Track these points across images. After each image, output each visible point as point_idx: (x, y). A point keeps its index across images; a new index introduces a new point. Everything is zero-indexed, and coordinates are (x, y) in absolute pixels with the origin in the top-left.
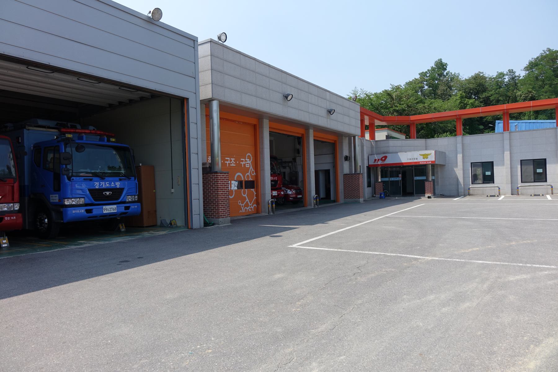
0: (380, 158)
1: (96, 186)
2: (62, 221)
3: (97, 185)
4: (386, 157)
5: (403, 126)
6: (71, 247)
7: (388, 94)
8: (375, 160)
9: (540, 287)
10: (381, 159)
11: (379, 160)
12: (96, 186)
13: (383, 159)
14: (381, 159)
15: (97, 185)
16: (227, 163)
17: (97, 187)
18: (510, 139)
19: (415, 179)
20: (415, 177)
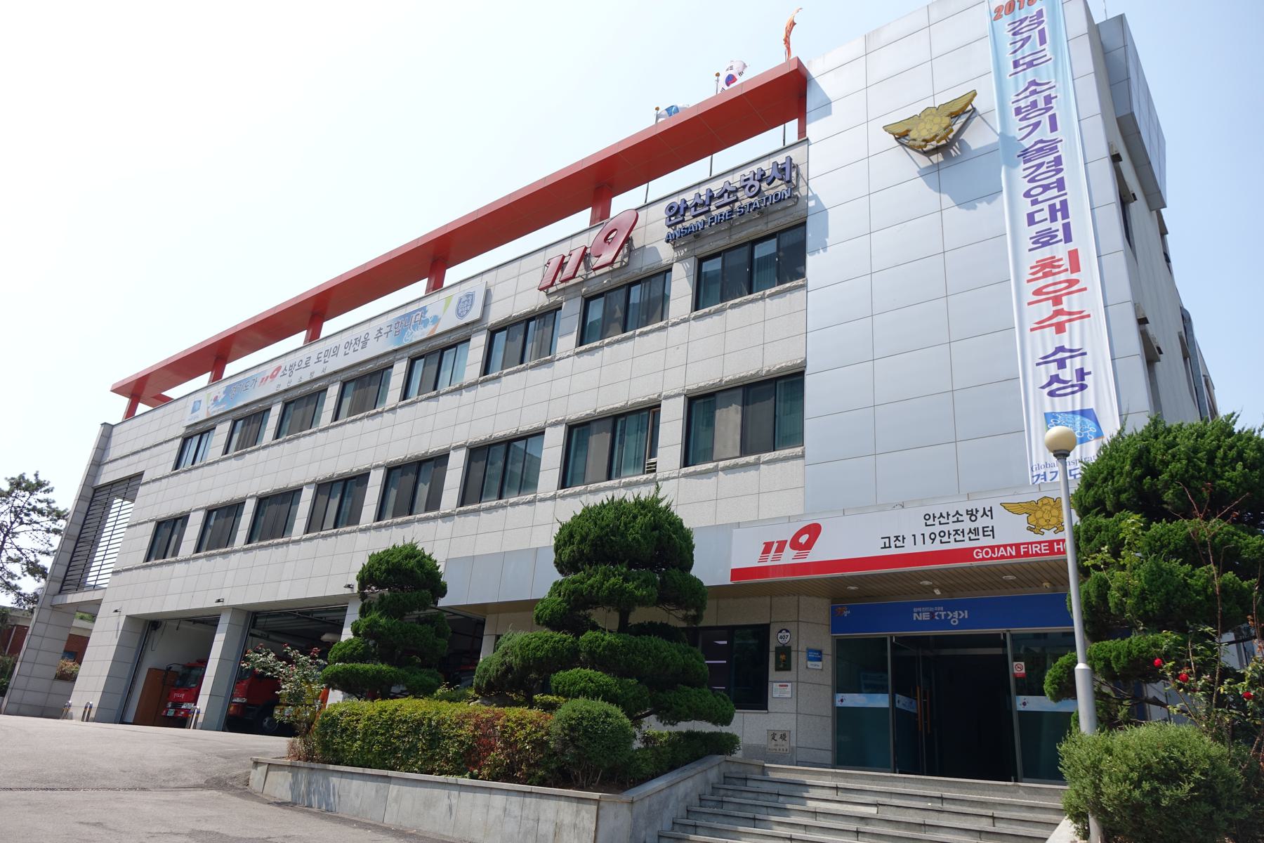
0: (789, 537)
1: (951, 619)
2: (694, 626)
3: (953, 617)
4: (814, 531)
5: (710, 226)
6: (345, 512)
7: (387, 551)
8: (768, 547)
9: (639, 759)
10: (795, 544)
11: (782, 545)
12: (951, 619)
13: (804, 539)
14: (795, 544)
15: (953, 617)
16: (1024, 552)
17: (955, 622)
18: (650, 287)
19: (1020, 708)
20: (1021, 699)
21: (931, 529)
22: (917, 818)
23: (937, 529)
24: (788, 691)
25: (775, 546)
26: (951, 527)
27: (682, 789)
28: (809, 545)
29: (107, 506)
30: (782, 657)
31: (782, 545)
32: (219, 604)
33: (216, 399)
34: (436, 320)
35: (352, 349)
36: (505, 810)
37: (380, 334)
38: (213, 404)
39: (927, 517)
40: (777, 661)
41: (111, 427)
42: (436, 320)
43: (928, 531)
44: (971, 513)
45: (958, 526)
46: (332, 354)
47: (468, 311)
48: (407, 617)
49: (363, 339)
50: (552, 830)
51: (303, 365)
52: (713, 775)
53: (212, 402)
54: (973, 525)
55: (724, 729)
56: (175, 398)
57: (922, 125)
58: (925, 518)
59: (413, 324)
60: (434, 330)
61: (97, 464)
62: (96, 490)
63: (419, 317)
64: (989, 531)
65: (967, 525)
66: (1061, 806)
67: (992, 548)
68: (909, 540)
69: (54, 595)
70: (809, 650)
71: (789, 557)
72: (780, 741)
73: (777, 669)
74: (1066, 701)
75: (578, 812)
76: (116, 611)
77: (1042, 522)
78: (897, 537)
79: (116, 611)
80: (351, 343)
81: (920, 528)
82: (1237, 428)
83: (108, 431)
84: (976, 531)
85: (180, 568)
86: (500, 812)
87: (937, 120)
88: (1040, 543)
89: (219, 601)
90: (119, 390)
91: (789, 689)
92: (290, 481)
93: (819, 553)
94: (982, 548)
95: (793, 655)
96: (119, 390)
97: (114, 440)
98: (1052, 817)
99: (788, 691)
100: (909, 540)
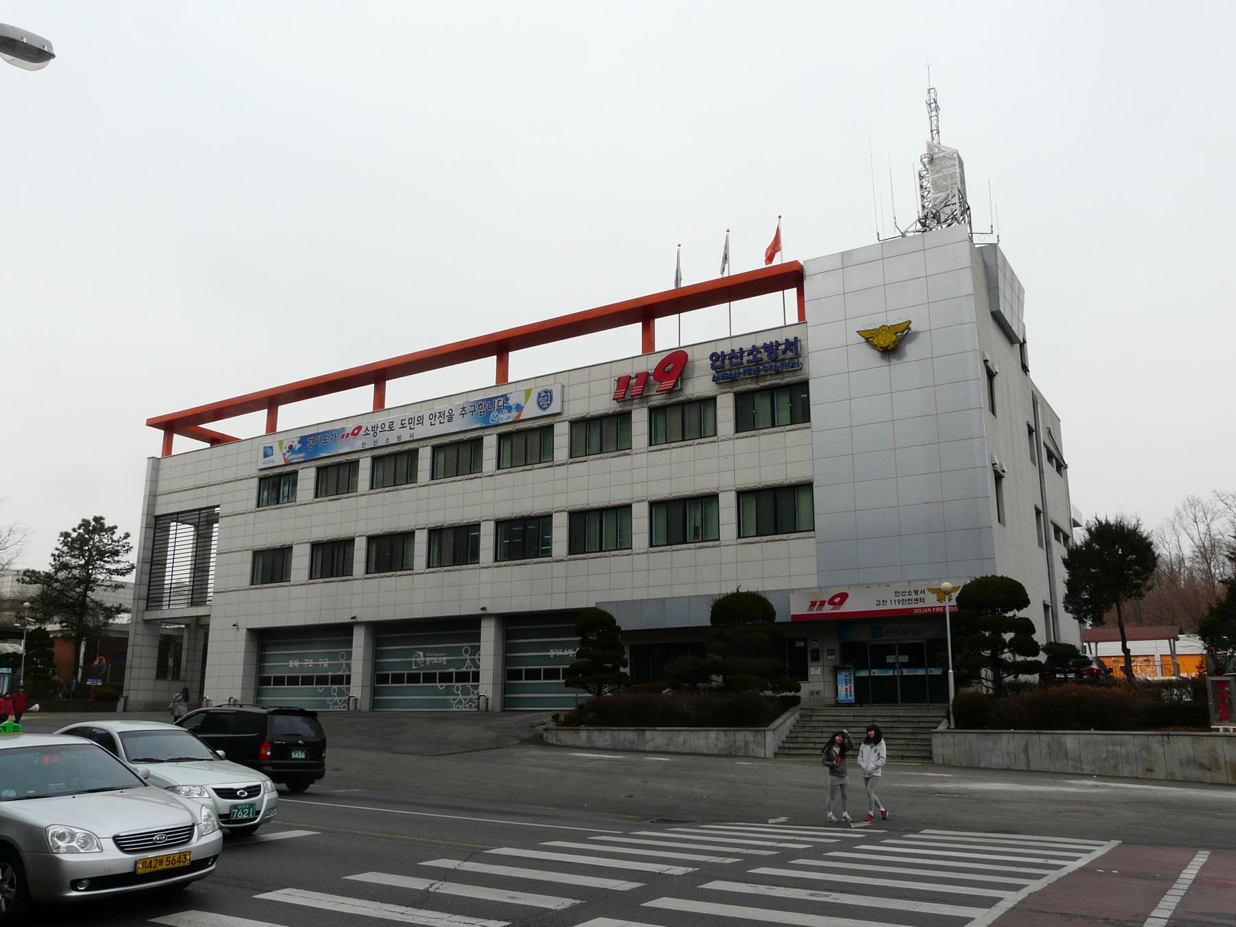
4: (844, 596)
8: (813, 604)
10: (831, 602)
11: (822, 603)
14: (831, 602)
21: (897, 598)
22: (890, 725)
23: (901, 598)
24: (819, 671)
25: (818, 603)
26: (907, 597)
27: (788, 723)
28: (841, 603)
29: (167, 530)
30: (815, 654)
31: (822, 603)
32: (354, 620)
33: (291, 447)
34: (519, 408)
35: (437, 421)
36: (717, 738)
37: (464, 412)
38: (288, 452)
39: (896, 592)
40: (812, 657)
41: (157, 461)
42: (519, 408)
43: (897, 598)
44: (916, 592)
45: (910, 597)
46: (416, 422)
47: (548, 405)
48: (188, 580)
49: (447, 414)
50: (743, 744)
51: (387, 428)
52: (797, 716)
53: (288, 449)
54: (916, 597)
55: (797, 694)
56: (243, 439)
57: (880, 337)
58: (384, 424)
59: (496, 407)
60: (519, 416)
61: (152, 496)
62: (157, 518)
63: (501, 403)
64: (922, 600)
65: (914, 596)
66: (943, 714)
67: (922, 608)
68: (889, 603)
69: (143, 611)
70: (828, 650)
71: (827, 609)
72: (816, 696)
73: (812, 661)
74: (277, 545)
75: (755, 736)
76: (234, 625)
77: (942, 598)
78: (883, 601)
79: (234, 625)
80: (436, 416)
81: (894, 598)
82: (1205, 652)
83: (155, 464)
84: (917, 600)
85: (295, 591)
86: (715, 740)
87: (889, 335)
88: (940, 607)
89: (352, 618)
90: (154, 423)
91: (819, 670)
92: (402, 525)
93: (848, 607)
94: (917, 608)
95: (821, 653)
96: (154, 423)
97: (163, 475)
98: (940, 719)
99: (819, 671)
100: (889, 603)
